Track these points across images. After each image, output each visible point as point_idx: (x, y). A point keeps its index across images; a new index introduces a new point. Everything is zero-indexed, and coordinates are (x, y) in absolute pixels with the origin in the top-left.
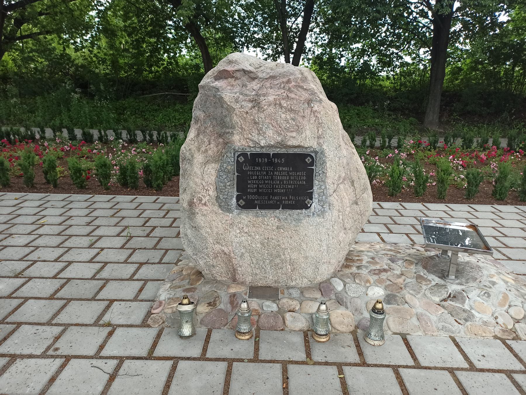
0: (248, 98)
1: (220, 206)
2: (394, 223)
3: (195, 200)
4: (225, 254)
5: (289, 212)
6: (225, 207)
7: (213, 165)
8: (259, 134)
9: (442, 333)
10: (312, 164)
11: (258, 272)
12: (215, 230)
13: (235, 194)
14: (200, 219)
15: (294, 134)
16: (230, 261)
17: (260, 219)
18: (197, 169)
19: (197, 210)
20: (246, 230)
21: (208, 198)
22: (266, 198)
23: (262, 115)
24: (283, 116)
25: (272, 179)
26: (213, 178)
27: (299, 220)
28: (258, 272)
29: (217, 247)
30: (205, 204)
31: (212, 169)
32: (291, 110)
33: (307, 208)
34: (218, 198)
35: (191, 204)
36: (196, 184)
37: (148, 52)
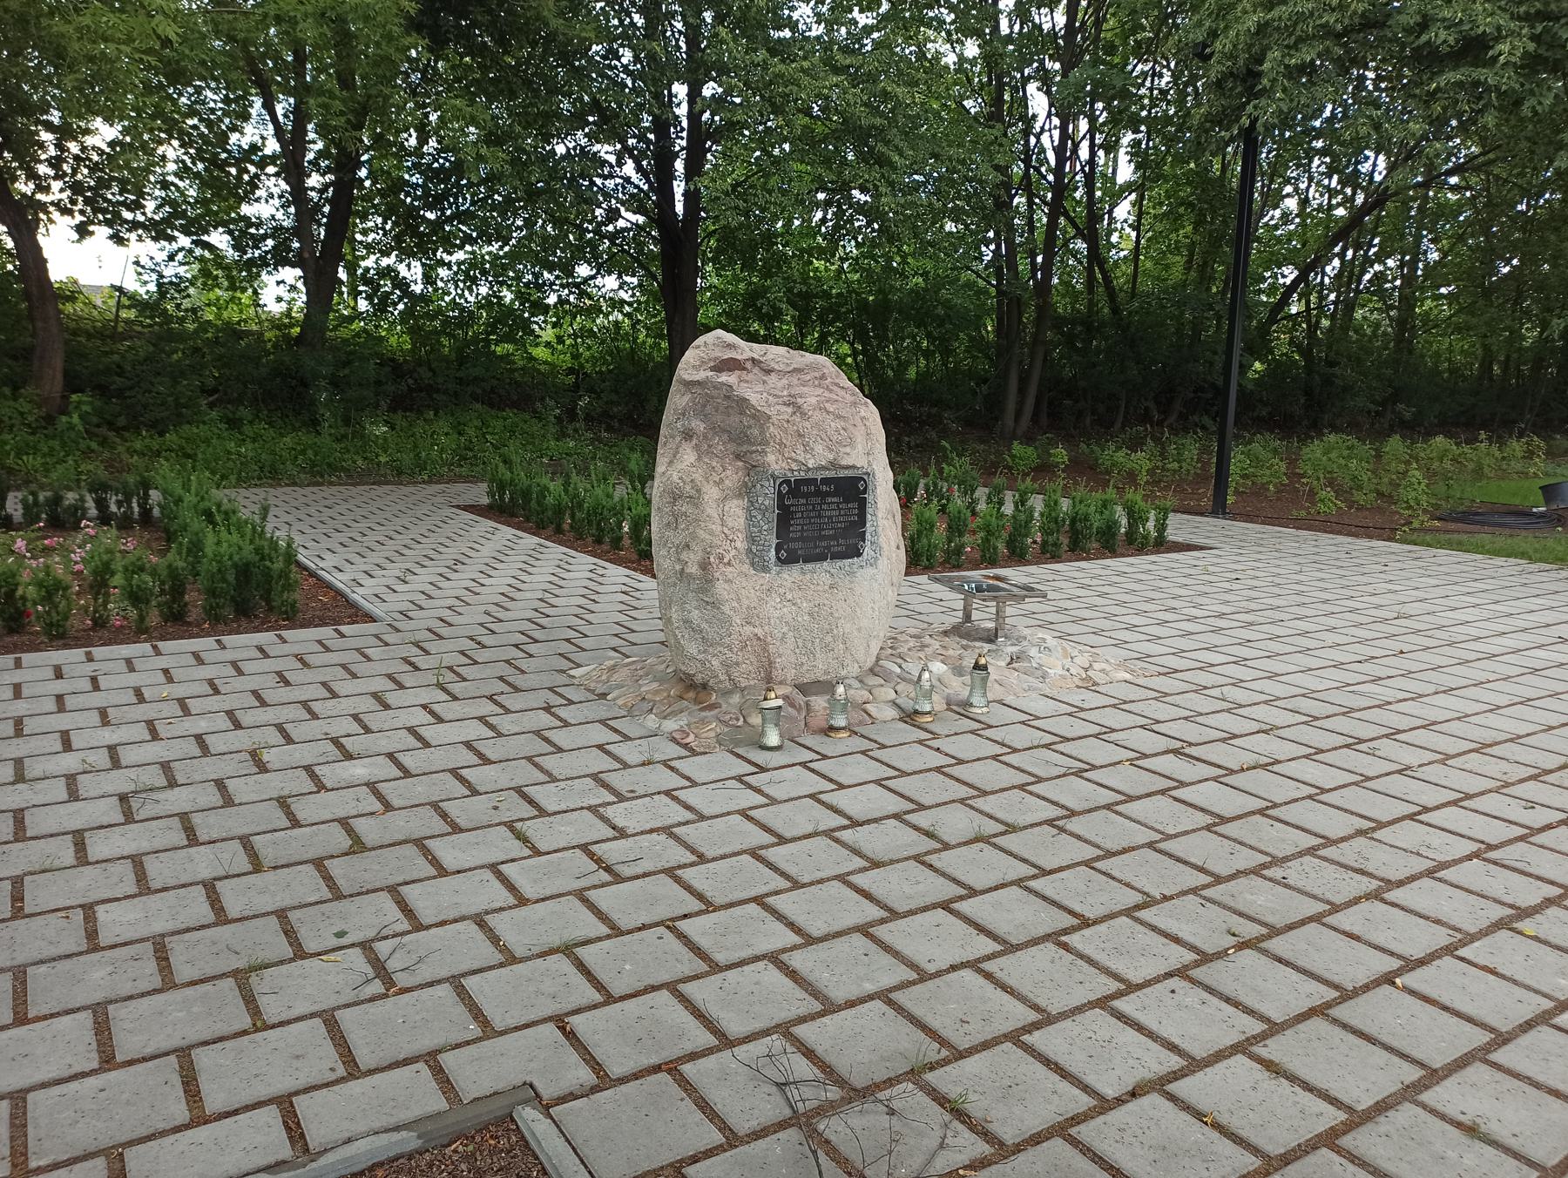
0: (780, 401)
1: (752, 564)
2: (821, 797)
3: (712, 560)
4: (759, 639)
5: (839, 563)
6: (759, 565)
7: (735, 501)
8: (806, 451)
9: (1030, 693)
10: (865, 491)
11: (804, 659)
12: (745, 602)
13: (775, 541)
14: (721, 588)
15: (848, 450)
16: (765, 650)
17: (808, 576)
18: (712, 510)
19: (717, 575)
20: (789, 596)
21: (733, 552)
22: (812, 545)
23: (807, 424)
24: (833, 424)
25: (820, 516)
26: (742, 520)
27: (852, 573)
28: (804, 659)
29: (748, 630)
30: (729, 564)
31: (736, 511)
32: (839, 417)
33: (859, 555)
34: (749, 551)
35: (705, 566)
36: (712, 533)
37: (1061, 358)
